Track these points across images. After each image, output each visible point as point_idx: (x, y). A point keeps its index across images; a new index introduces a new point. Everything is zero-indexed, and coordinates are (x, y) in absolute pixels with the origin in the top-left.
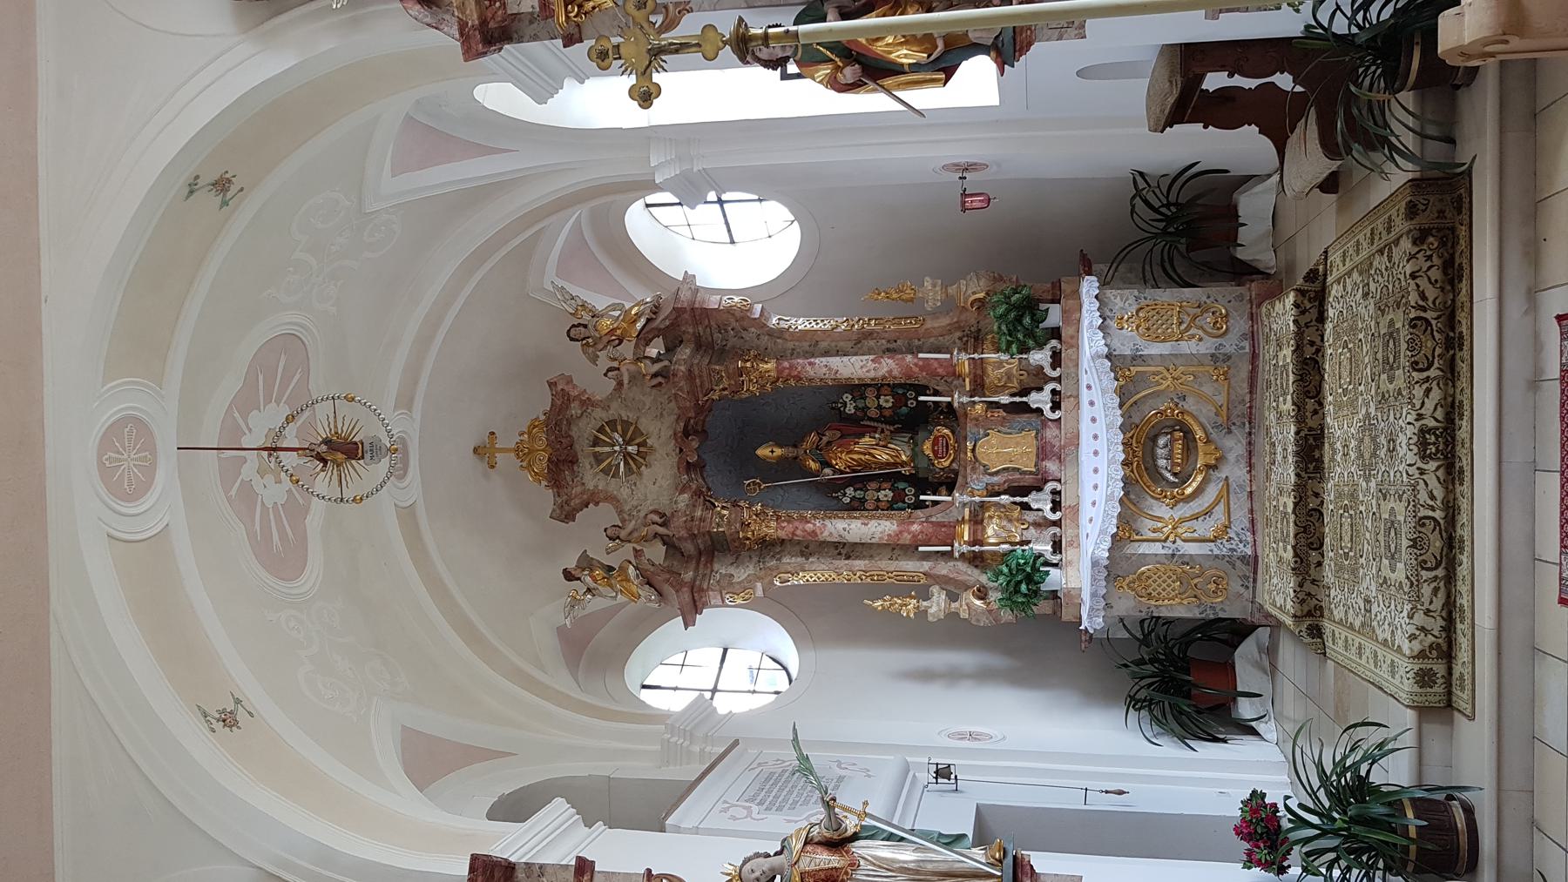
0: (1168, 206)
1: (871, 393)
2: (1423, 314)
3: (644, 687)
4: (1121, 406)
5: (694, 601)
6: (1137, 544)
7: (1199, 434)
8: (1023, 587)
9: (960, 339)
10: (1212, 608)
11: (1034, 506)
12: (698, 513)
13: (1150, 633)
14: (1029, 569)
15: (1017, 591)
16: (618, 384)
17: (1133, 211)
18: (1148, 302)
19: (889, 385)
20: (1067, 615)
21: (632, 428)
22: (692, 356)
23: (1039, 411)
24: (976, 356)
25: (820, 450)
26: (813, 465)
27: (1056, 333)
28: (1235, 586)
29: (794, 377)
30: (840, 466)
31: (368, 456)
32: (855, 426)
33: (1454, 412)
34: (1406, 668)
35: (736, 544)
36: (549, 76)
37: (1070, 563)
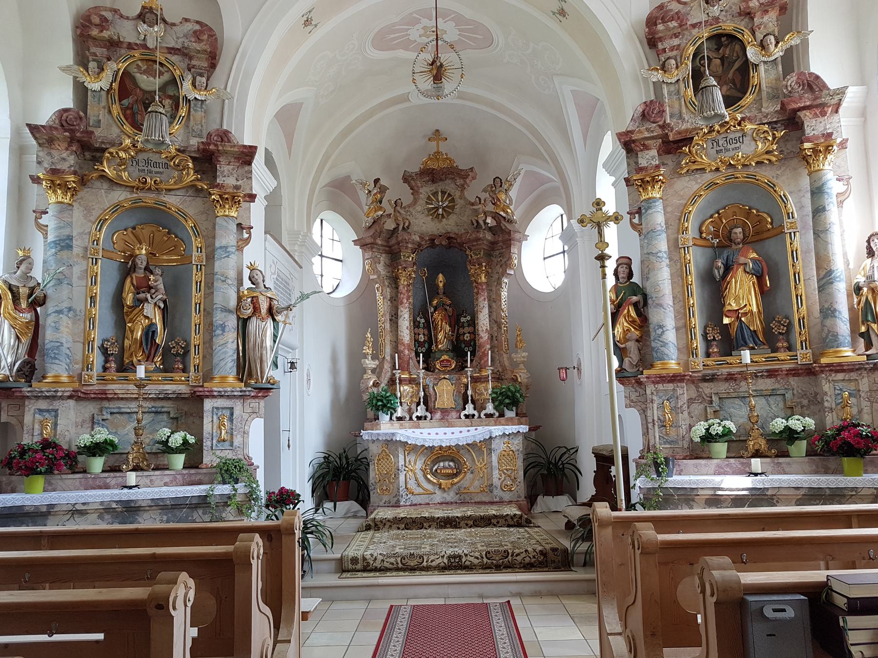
0: (562, 464)
1: (471, 329)
2: (510, 555)
3: (322, 220)
4: (468, 444)
5: (367, 245)
6: (403, 453)
7: (455, 480)
8: (380, 403)
9: (498, 371)
10: (374, 489)
11: (419, 408)
12: (410, 246)
13: (362, 462)
14: (389, 405)
15: (378, 400)
16: (473, 203)
17: (560, 447)
18: (516, 455)
19: (475, 338)
20: (366, 425)
21: (451, 211)
22: (487, 240)
23: (464, 409)
24: (490, 378)
25: (442, 306)
26: (435, 302)
27: (502, 415)
28: (385, 498)
29: (478, 291)
30: (435, 316)
31: (435, 85)
32: (455, 322)
33: (469, 568)
34: (359, 554)
35: (395, 265)
36: (614, 170)
37: (392, 425)
